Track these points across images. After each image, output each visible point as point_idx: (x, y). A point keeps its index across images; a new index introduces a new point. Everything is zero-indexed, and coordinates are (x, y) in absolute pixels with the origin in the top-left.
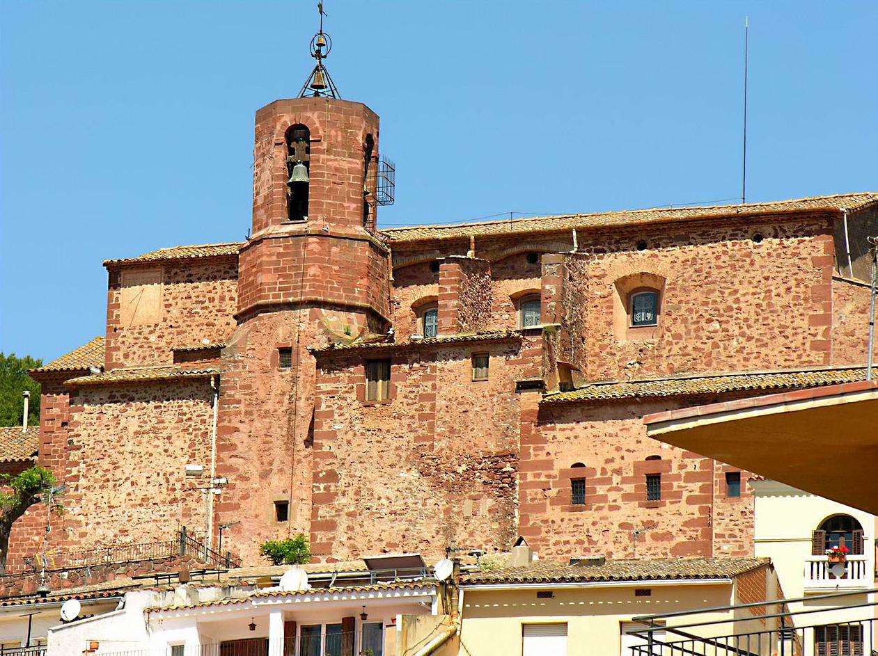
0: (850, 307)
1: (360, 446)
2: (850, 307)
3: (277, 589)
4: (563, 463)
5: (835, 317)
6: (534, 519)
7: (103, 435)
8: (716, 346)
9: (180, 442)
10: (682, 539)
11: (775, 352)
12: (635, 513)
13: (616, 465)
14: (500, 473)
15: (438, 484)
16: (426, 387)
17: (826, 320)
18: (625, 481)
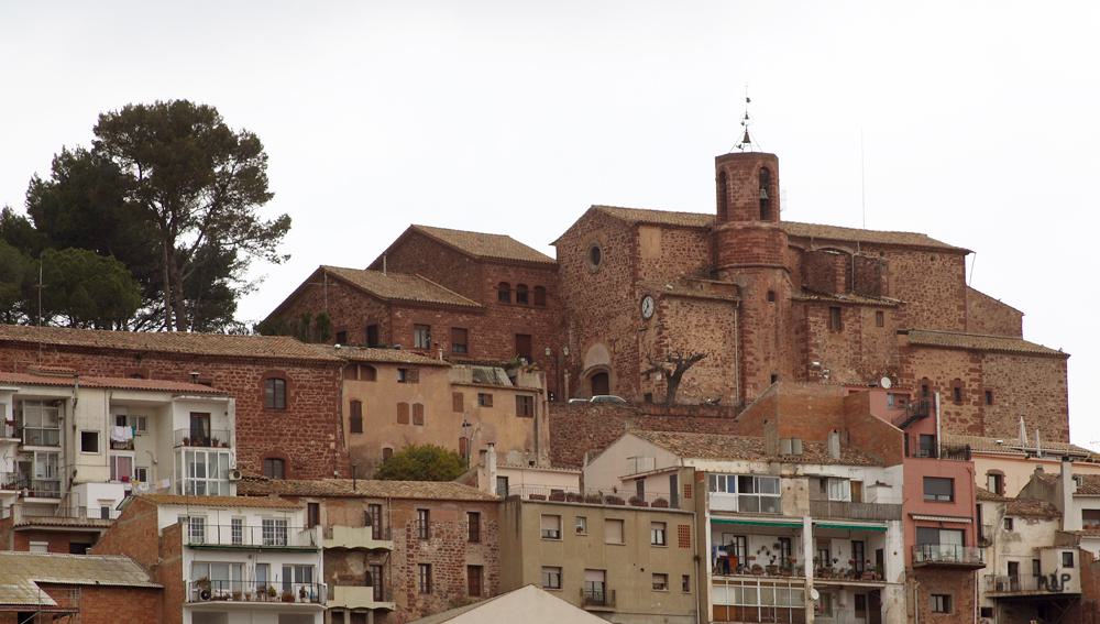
0: (974, 304)
2: (974, 304)
3: (482, 391)
4: (919, 376)
5: (968, 307)
7: (679, 324)
8: (917, 314)
9: (719, 334)
10: (972, 423)
13: (941, 381)
16: (857, 326)
18: (946, 389)
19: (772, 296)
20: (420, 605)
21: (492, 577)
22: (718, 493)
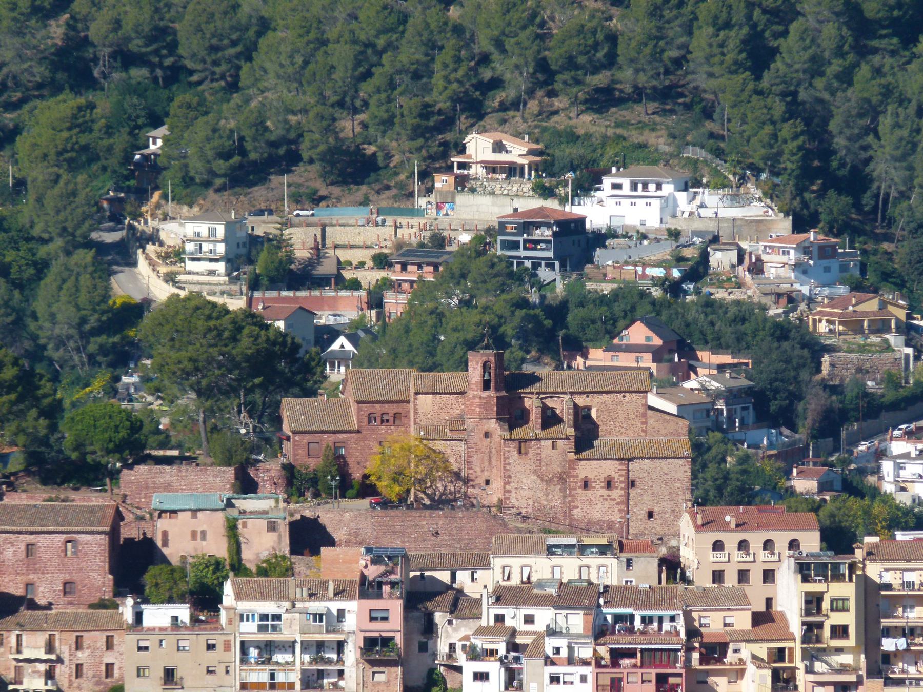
1: (519, 468)
4: (582, 476)
6: (573, 492)
11: (630, 432)
12: (605, 492)
14: (562, 479)
15: (542, 480)
17: (645, 423)
19: (487, 435)
20: (75, 685)
21: (120, 668)
22: (245, 623)
